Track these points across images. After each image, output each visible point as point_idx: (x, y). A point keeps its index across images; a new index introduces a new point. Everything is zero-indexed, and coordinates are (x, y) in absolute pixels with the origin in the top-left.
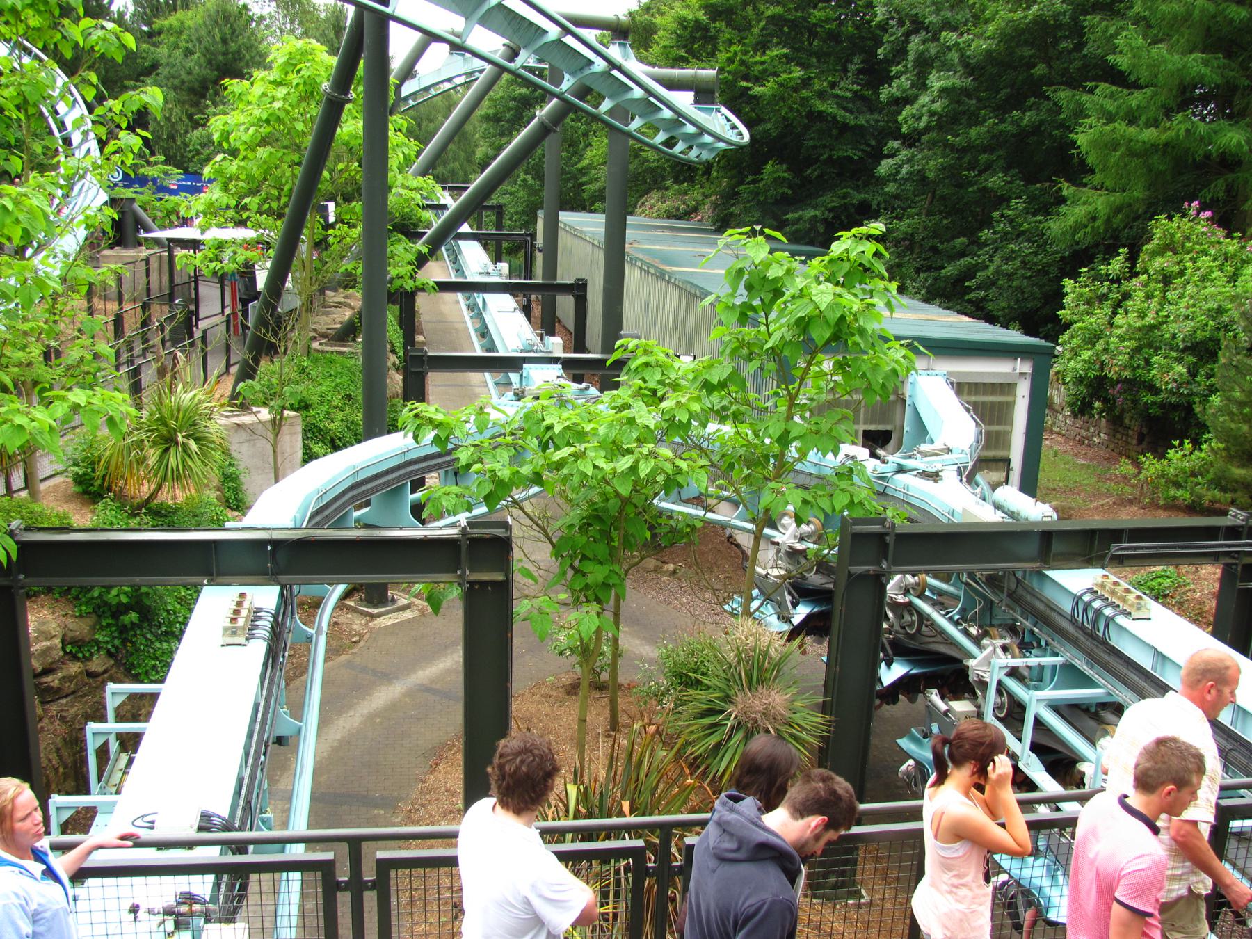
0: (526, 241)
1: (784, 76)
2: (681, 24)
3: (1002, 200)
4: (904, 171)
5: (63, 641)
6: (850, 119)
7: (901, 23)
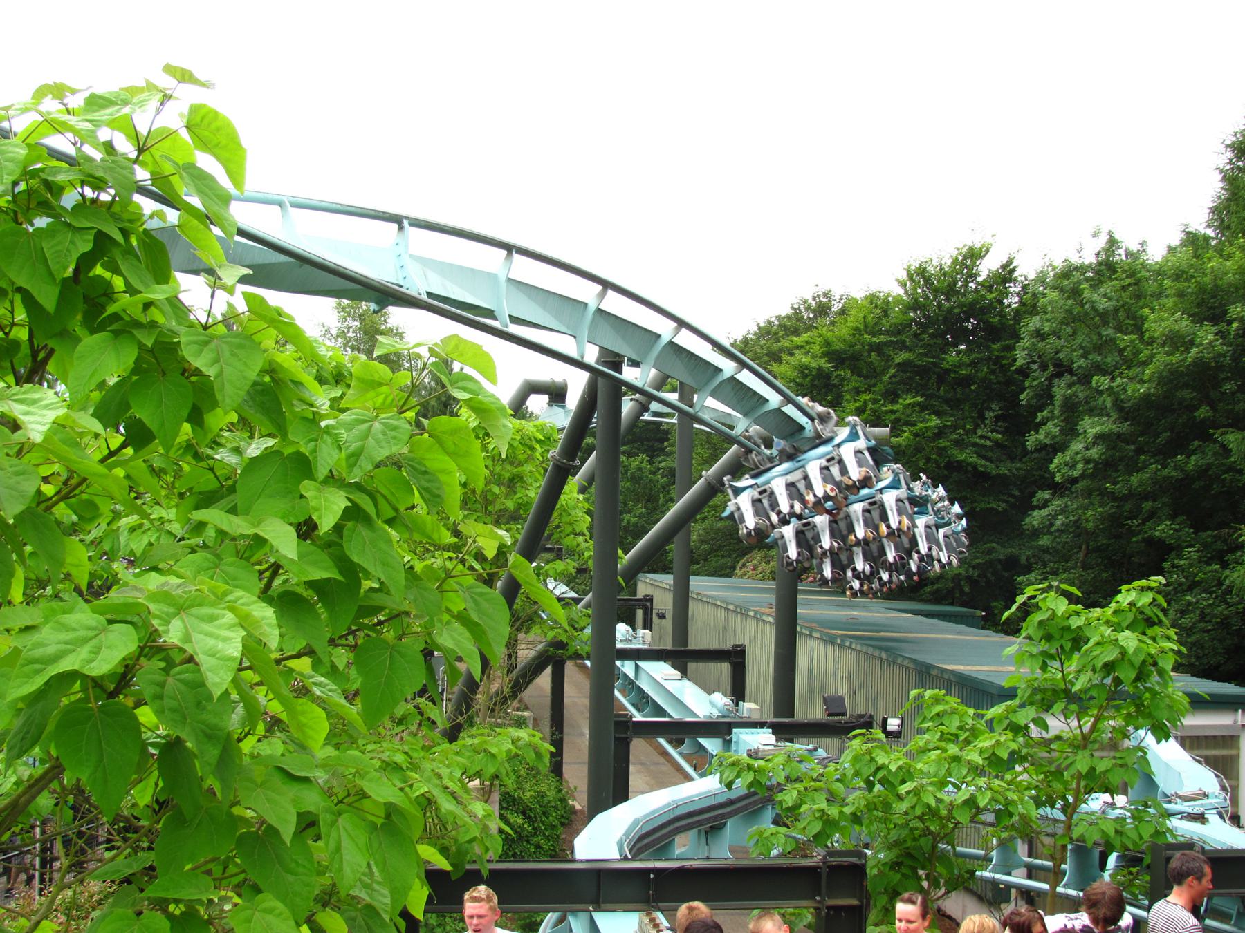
1: (921, 425)
2: (802, 372)
3: (1176, 549)
4: (1059, 522)
6: (991, 468)
7: (1044, 367)
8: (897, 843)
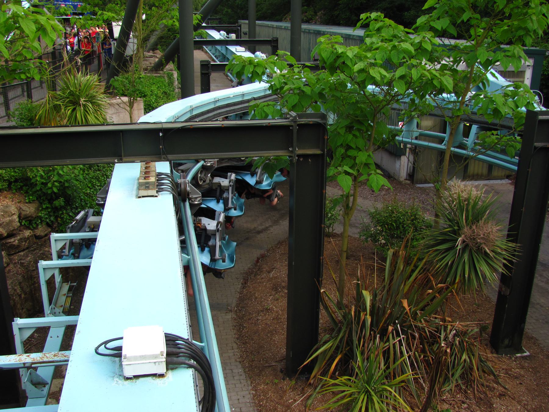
0: (238, 29)
5: (19, 217)
8: (348, 116)
